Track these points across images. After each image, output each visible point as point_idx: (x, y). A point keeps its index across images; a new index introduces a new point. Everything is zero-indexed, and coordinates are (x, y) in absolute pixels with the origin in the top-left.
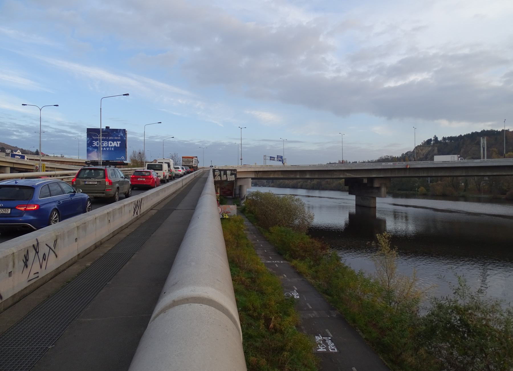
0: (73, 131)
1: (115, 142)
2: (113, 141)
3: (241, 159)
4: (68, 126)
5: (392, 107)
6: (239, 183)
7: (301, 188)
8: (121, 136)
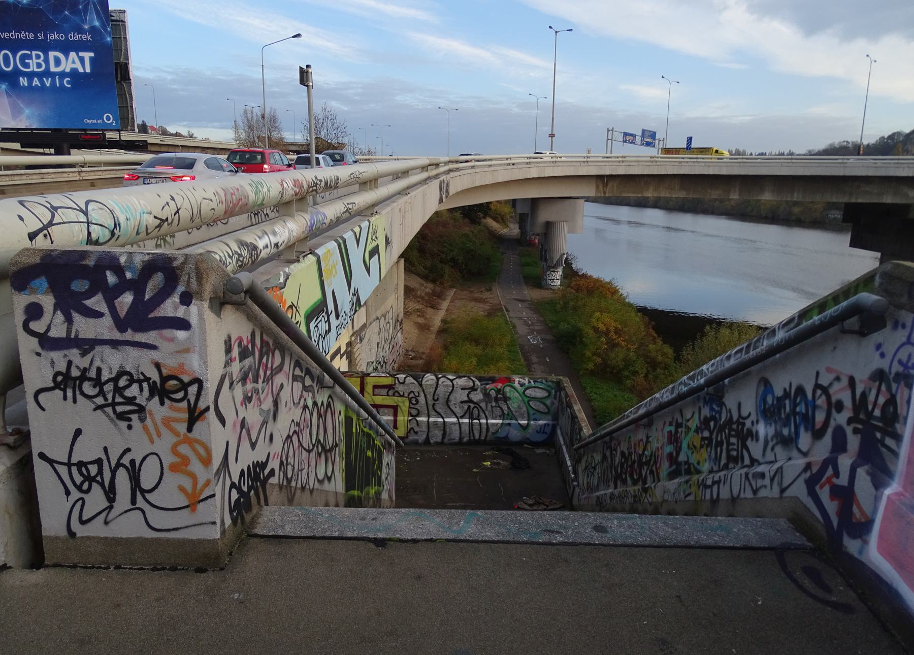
1: (73, 55)
2: (66, 48)
3: (552, 136)
6: (545, 215)
8: (93, 30)
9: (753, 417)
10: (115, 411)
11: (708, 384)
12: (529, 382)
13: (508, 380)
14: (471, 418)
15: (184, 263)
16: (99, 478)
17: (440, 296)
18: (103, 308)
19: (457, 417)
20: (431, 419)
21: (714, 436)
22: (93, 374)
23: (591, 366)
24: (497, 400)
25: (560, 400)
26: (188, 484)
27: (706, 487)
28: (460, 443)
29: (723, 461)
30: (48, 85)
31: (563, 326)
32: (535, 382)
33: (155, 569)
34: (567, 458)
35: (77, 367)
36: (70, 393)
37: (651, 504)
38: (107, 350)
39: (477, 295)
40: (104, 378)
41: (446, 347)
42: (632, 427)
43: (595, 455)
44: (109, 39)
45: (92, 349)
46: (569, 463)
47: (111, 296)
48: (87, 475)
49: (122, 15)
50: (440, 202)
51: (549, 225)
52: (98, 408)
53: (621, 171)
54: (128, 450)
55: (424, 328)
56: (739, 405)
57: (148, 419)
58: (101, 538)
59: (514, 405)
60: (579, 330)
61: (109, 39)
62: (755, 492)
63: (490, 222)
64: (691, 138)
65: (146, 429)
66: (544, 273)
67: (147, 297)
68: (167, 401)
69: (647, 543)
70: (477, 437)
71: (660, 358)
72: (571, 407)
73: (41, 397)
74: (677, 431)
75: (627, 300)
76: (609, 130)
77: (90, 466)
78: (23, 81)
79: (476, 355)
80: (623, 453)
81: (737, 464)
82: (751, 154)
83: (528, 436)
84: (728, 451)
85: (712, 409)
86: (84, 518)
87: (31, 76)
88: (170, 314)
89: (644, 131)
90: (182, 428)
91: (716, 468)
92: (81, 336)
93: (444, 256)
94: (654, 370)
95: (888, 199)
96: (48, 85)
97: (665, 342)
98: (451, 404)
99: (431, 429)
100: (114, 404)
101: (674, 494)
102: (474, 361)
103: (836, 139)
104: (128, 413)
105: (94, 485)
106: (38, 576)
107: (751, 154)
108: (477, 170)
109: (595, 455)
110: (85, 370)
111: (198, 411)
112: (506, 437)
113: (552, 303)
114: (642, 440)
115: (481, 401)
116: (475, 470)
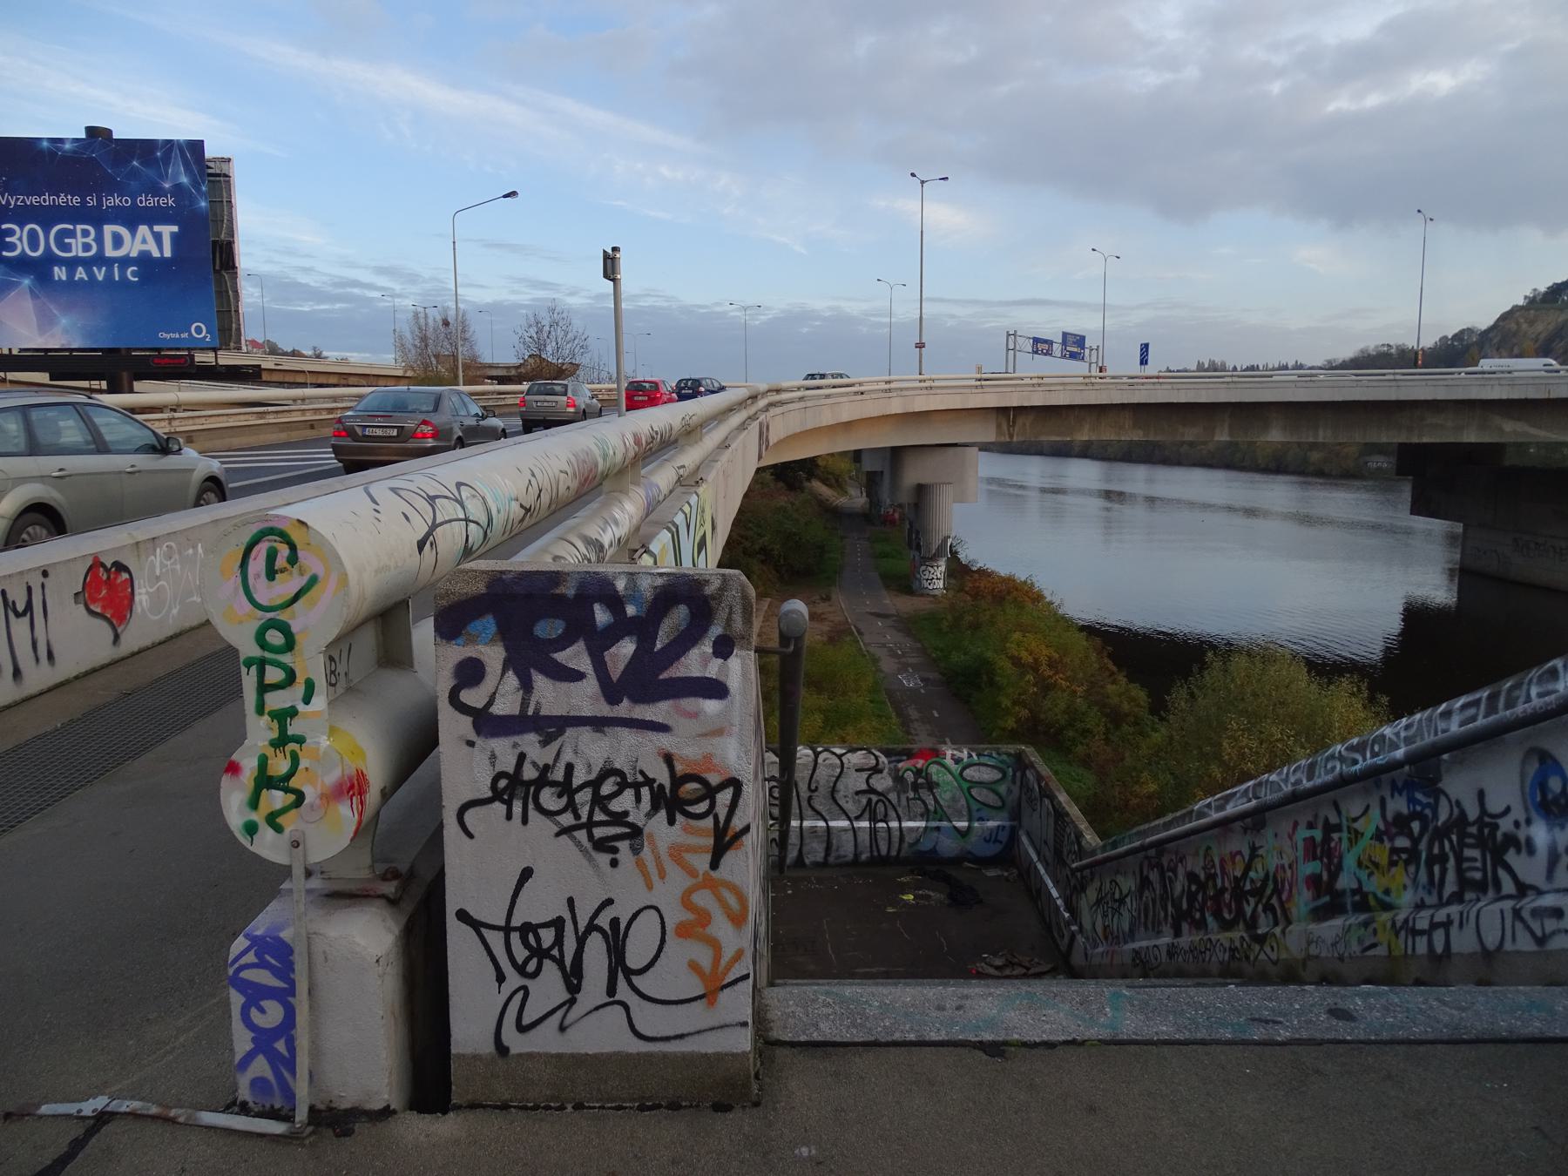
0: (382, 281)
1: (143, 230)
2: (132, 218)
3: (920, 346)
4: (366, 267)
6: (914, 474)
8: (178, 190)
9: (1518, 813)
10: (590, 836)
11: (1411, 759)
12: (970, 756)
13: (934, 754)
14: (873, 819)
15: (722, 589)
16: (555, 952)
18: (584, 663)
19: (849, 819)
20: (806, 824)
21: (1423, 846)
22: (558, 775)
23: (1011, 723)
24: (916, 787)
25: (1024, 785)
26: (704, 957)
27: (1415, 933)
28: (856, 863)
29: (1450, 887)
30: (100, 278)
31: (957, 658)
32: (979, 755)
33: (642, 1108)
34: (1050, 884)
35: (534, 764)
36: (517, 808)
37: (1275, 963)
38: (585, 734)
40: (577, 781)
42: (1215, 831)
43: (1120, 879)
44: (203, 204)
45: (561, 732)
46: (1055, 893)
47: (599, 643)
48: (535, 947)
49: (224, 166)
50: (760, 457)
51: (922, 490)
52: (565, 831)
53: (1037, 400)
54: (609, 902)
56: (1481, 795)
57: (646, 850)
58: (552, 1056)
59: (944, 796)
61: (203, 204)
62: (1541, 941)
63: (818, 486)
64: (1147, 346)
65: (641, 865)
67: (659, 646)
68: (679, 818)
69: (1431, 1036)
70: (884, 851)
71: (1126, 707)
72: (1052, 798)
73: (469, 816)
74: (1327, 839)
75: (1061, 612)
77: (542, 932)
78: (60, 273)
80: (1191, 877)
81: (1485, 891)
82: (1235, 369)
83: (969, 847)
84: (1460, 872)
85: (1412, 800)
86: (526, 1021)
87: (72, 264)
88: (696, 673)
89: (1065, 335)
90: (702, 862)
91: (1430, 900)
92: (542, 713)
93: (747, 544)
94: (1118, 727)
95: (1471, 436)
96: (100, 278)
97: (1131, 680)
98: (839, 796)
99: (807, 841)
100: (590, 825)
101: (1334, 945)
102: (818, 719)
103: (1372, 344)
104: (610, 837)
105: (547, 963)
106: (445, 1127)
107: (1235, 369)
108: (809, 404)
109: (1120, 879)
110: (547, 768)
111: (730, 833)
112: (934, 851)
114: (1240, 853)
115: (889, 790)
116: (890, 910)
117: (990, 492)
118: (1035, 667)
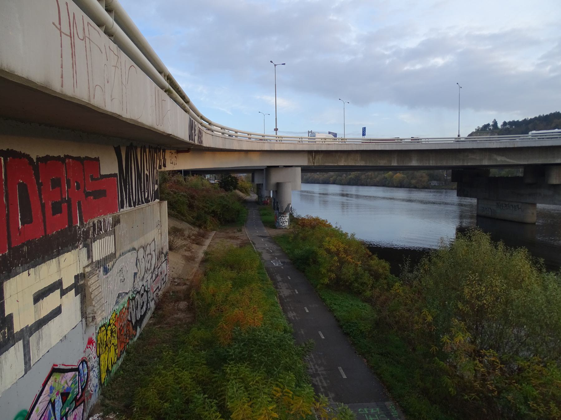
5: (416, 95)
6: (275, 178)
7: (334, 183)
17: (204, 236)
23: (326, 281)
31: (297, 252)
39: (231, 235)
41: (205, 274)
55: (190, 259)
60: (314, 253)
66: (277, 218)
71: (381, 271)
76: (309, 132)
79: (231, 279)
93: (207, 210)
95: (486, 163)
102: (230, 283)
113: (284, 237)
117: (301, 195)
118: (337, 253)
